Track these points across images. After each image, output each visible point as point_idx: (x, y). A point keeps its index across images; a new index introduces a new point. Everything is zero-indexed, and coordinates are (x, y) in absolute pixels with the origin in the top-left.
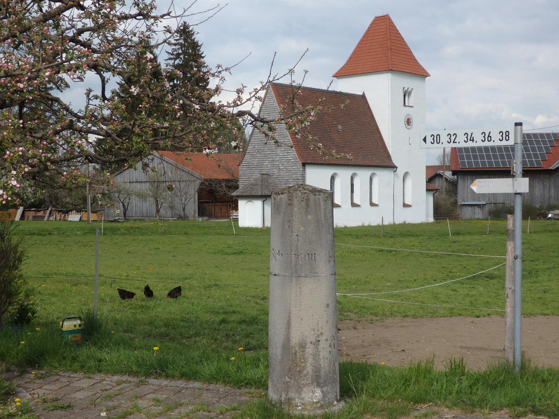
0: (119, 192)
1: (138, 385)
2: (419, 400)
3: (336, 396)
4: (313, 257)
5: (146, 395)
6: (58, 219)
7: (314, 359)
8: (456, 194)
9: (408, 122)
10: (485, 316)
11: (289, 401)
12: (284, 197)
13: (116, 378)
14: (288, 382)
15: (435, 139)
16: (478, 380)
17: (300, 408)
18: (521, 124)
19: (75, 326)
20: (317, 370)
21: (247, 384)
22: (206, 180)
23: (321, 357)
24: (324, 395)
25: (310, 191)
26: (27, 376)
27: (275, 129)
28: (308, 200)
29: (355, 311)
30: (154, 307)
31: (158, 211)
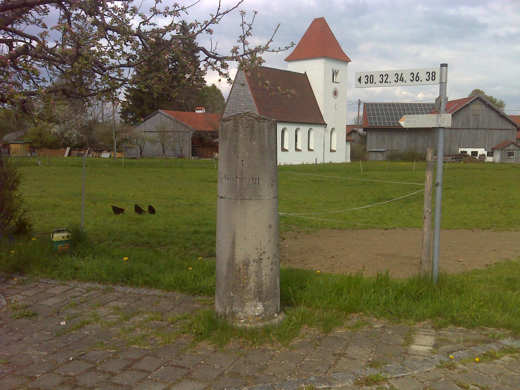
0: (137, 138)
1: (105, 292)
2: (351, 310)
3: (277, 309)
4: (257, 181)
5: (108, 303)
6: (94, 156)
7: (256, 276)
8: (365, 143)
9: (335, 93)
10: (391, 229)
11: (233, 314)
12: (230, 123)
13: (87, 285)
14: (232, 297)
15: (369, 79)
16: (402, 292)
17: (243, 321)
18: (446, 65)
19: (63, 237)
20: (259, 286)
21: (201, 292)
22: (197, 131)
23: (263, 274)
24: (266, 308)
25: (255, 118)
26: (11, 282)
27: (227, 66)
28: (252, 127)
29: (296, 224)
30: (147, 219)
31: (164, 152)
